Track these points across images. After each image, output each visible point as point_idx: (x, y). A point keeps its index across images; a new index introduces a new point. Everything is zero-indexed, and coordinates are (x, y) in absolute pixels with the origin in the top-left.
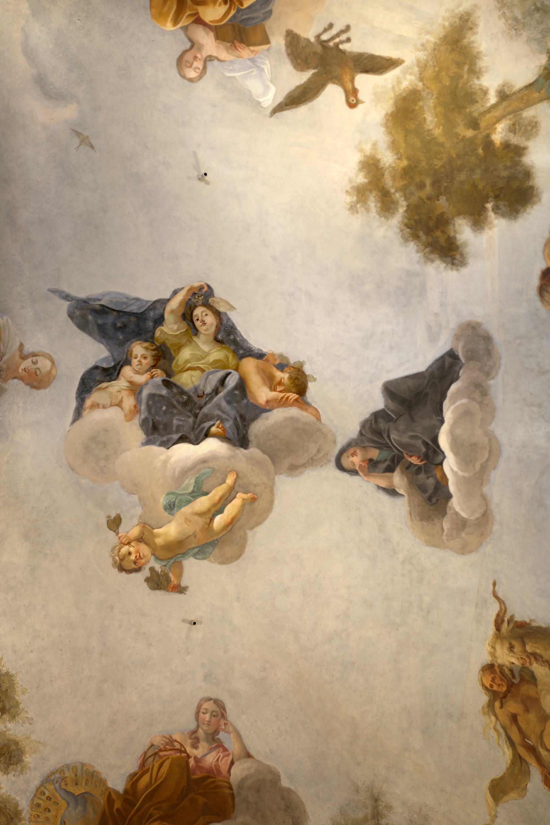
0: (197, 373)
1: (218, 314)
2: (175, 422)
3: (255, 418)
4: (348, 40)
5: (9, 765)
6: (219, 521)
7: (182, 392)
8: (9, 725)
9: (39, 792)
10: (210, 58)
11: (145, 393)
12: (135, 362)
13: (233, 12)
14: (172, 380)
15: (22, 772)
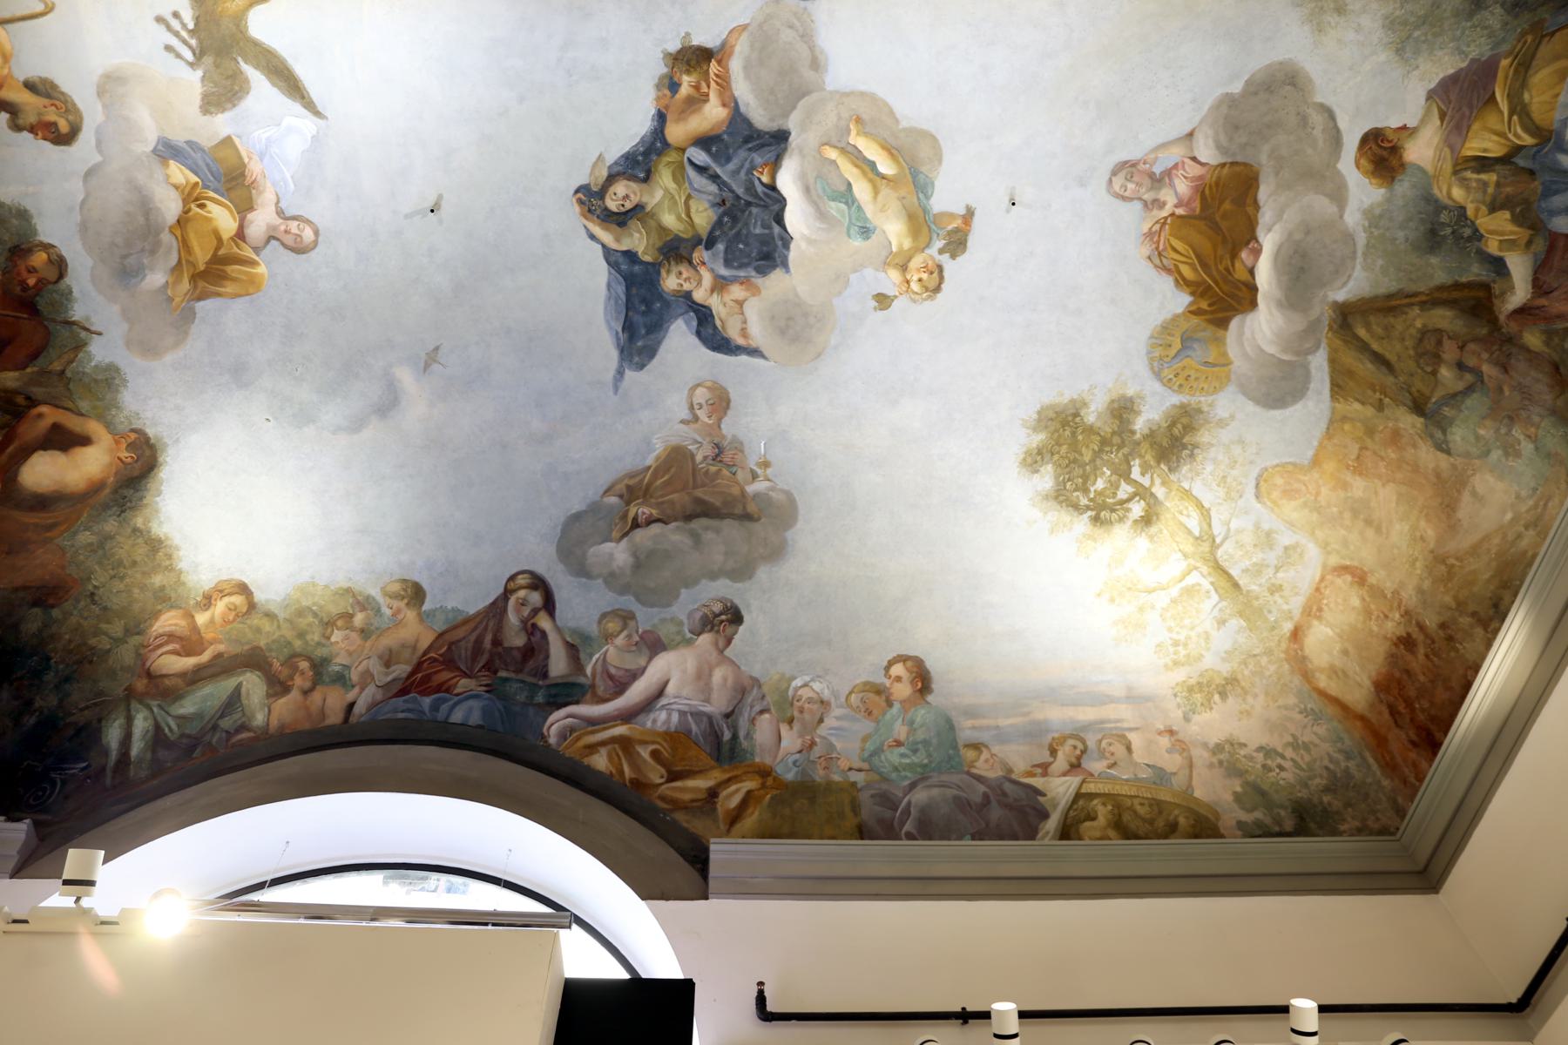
0: (692, 203)
1: (612, 179)
2: (758, 231)
3: (747, 122)
4: (176, 15)
5: (1132, 410)
6: (886, 167)
7: (719, 224)
8: (1093, 408)
9: (1167, 383)
10: (280, 213)
11: (724, 272)
12: (687, 286)
13: (211, 194)
14: (705, 237)
15: (1142, 398)
